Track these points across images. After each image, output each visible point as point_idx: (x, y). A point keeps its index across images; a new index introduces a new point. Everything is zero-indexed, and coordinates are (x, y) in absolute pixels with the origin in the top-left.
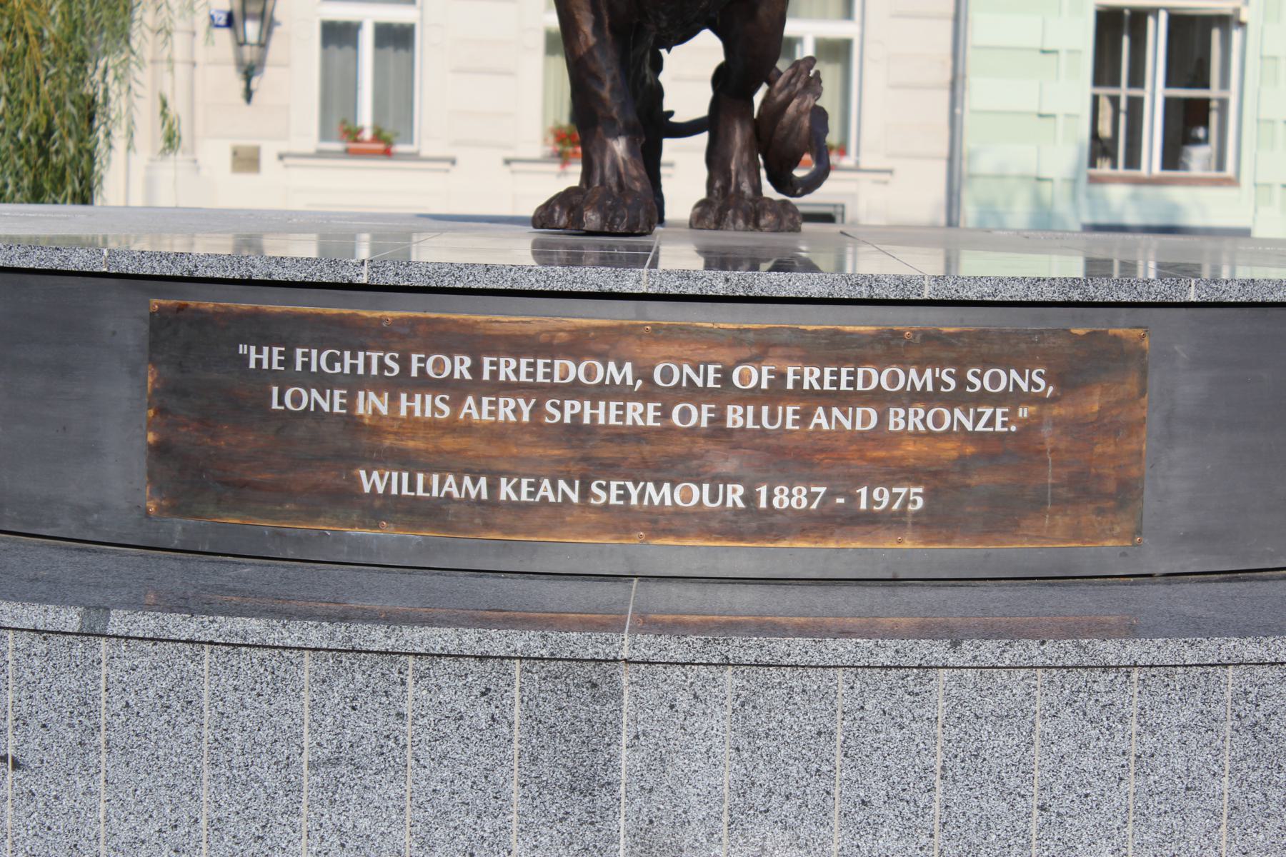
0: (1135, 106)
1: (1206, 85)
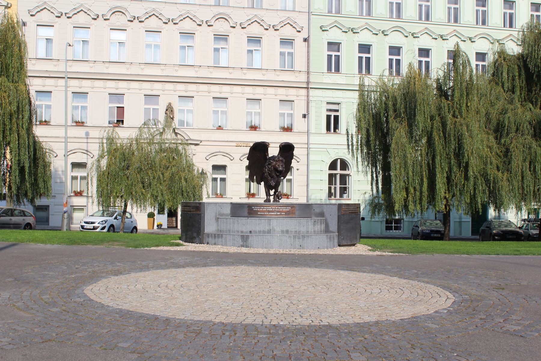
0: (335, 188)
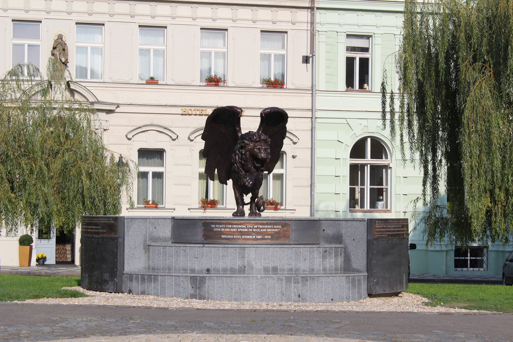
0: (362, 191)
1: (382, 185)
